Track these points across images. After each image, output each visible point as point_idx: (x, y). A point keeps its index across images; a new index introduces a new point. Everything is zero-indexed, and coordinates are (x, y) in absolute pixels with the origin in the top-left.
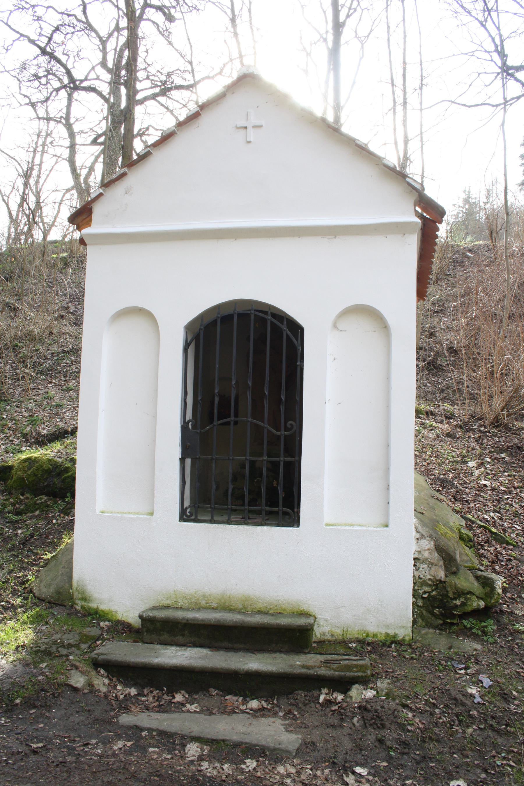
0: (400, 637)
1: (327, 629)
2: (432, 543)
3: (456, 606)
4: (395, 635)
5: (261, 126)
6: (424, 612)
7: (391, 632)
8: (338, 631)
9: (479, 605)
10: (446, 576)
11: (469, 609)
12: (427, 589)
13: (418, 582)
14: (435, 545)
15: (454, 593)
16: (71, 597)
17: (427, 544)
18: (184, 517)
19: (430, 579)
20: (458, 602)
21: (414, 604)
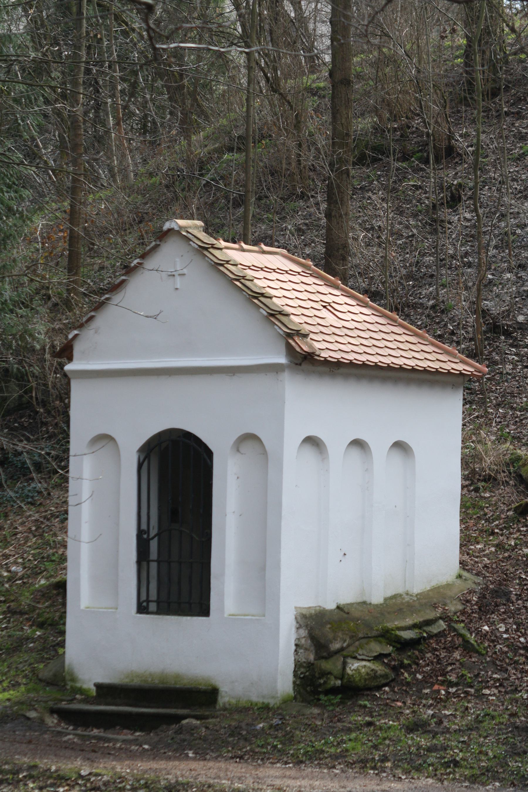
0: (271, 706)
1: (226, 699)
2: (307, 632)
3: (320, 685)
4: (269, 704)
5: (184, 275)
6: (302, 690)
7: (266, 701)
8: (234, 701)
9: (335, 684)
10: (315, 659)
11: (329, 686)
12: (302, 670)
13: (298, 665)
14: (308, 633)
15: (319, 674)
16: (64, 679)
17: (303, 632)
18: (142, 608)
19: (304, 662)
20: (322, 681)
21: (294, 683)
